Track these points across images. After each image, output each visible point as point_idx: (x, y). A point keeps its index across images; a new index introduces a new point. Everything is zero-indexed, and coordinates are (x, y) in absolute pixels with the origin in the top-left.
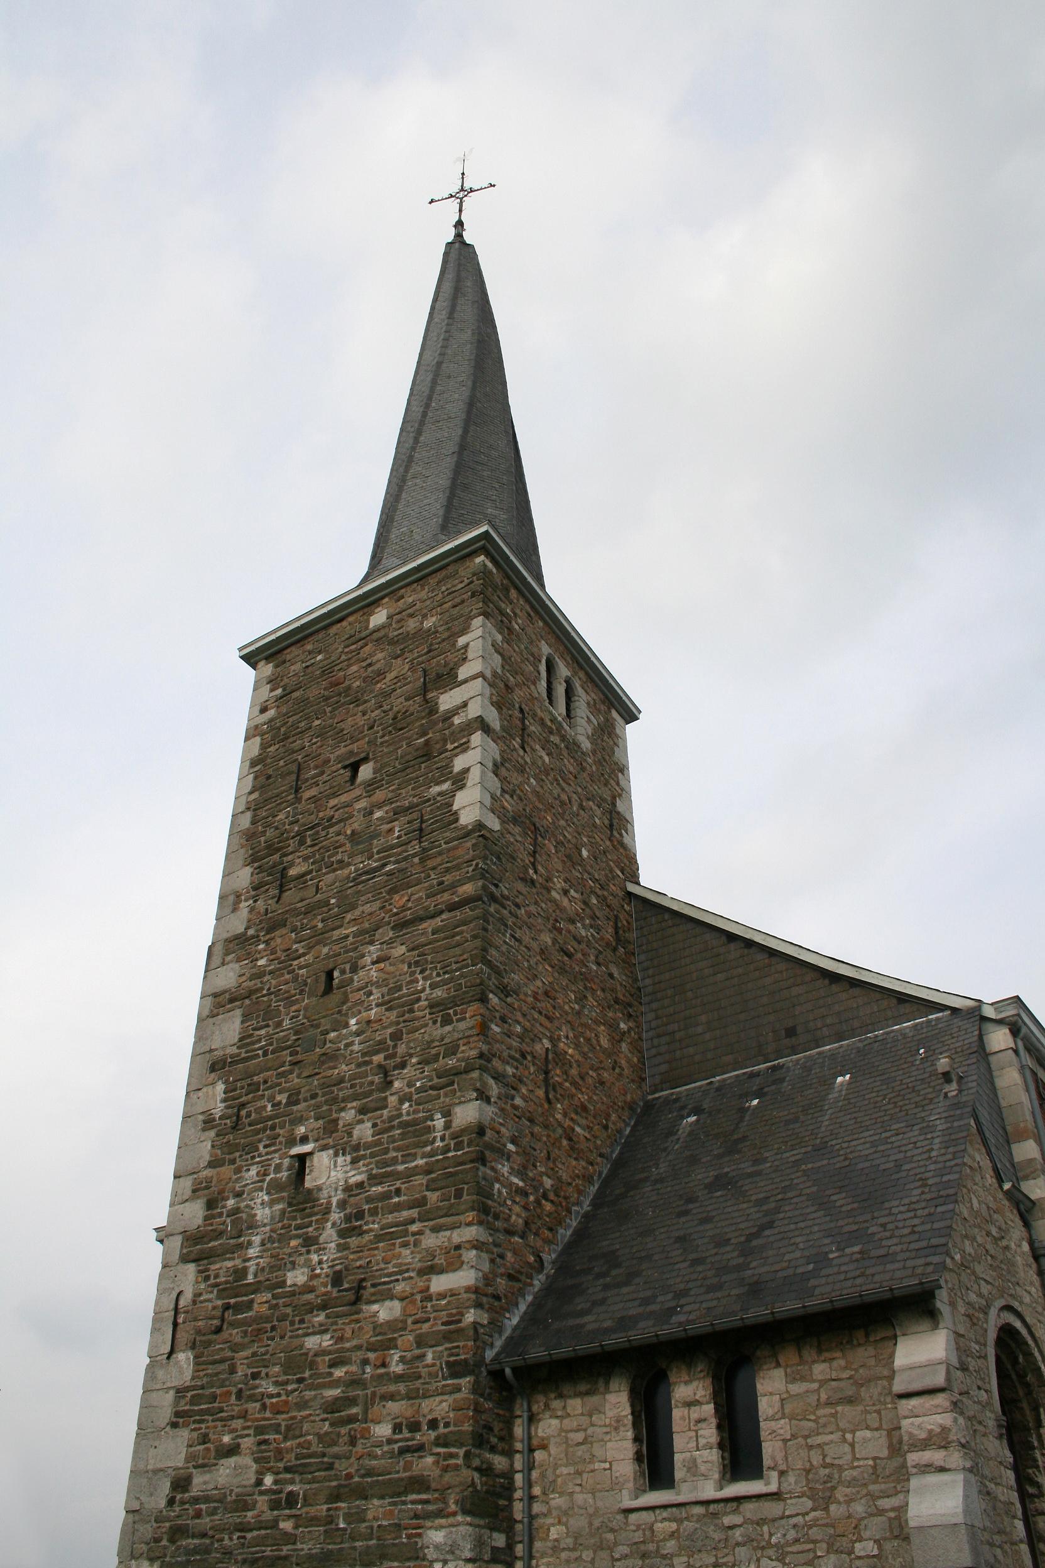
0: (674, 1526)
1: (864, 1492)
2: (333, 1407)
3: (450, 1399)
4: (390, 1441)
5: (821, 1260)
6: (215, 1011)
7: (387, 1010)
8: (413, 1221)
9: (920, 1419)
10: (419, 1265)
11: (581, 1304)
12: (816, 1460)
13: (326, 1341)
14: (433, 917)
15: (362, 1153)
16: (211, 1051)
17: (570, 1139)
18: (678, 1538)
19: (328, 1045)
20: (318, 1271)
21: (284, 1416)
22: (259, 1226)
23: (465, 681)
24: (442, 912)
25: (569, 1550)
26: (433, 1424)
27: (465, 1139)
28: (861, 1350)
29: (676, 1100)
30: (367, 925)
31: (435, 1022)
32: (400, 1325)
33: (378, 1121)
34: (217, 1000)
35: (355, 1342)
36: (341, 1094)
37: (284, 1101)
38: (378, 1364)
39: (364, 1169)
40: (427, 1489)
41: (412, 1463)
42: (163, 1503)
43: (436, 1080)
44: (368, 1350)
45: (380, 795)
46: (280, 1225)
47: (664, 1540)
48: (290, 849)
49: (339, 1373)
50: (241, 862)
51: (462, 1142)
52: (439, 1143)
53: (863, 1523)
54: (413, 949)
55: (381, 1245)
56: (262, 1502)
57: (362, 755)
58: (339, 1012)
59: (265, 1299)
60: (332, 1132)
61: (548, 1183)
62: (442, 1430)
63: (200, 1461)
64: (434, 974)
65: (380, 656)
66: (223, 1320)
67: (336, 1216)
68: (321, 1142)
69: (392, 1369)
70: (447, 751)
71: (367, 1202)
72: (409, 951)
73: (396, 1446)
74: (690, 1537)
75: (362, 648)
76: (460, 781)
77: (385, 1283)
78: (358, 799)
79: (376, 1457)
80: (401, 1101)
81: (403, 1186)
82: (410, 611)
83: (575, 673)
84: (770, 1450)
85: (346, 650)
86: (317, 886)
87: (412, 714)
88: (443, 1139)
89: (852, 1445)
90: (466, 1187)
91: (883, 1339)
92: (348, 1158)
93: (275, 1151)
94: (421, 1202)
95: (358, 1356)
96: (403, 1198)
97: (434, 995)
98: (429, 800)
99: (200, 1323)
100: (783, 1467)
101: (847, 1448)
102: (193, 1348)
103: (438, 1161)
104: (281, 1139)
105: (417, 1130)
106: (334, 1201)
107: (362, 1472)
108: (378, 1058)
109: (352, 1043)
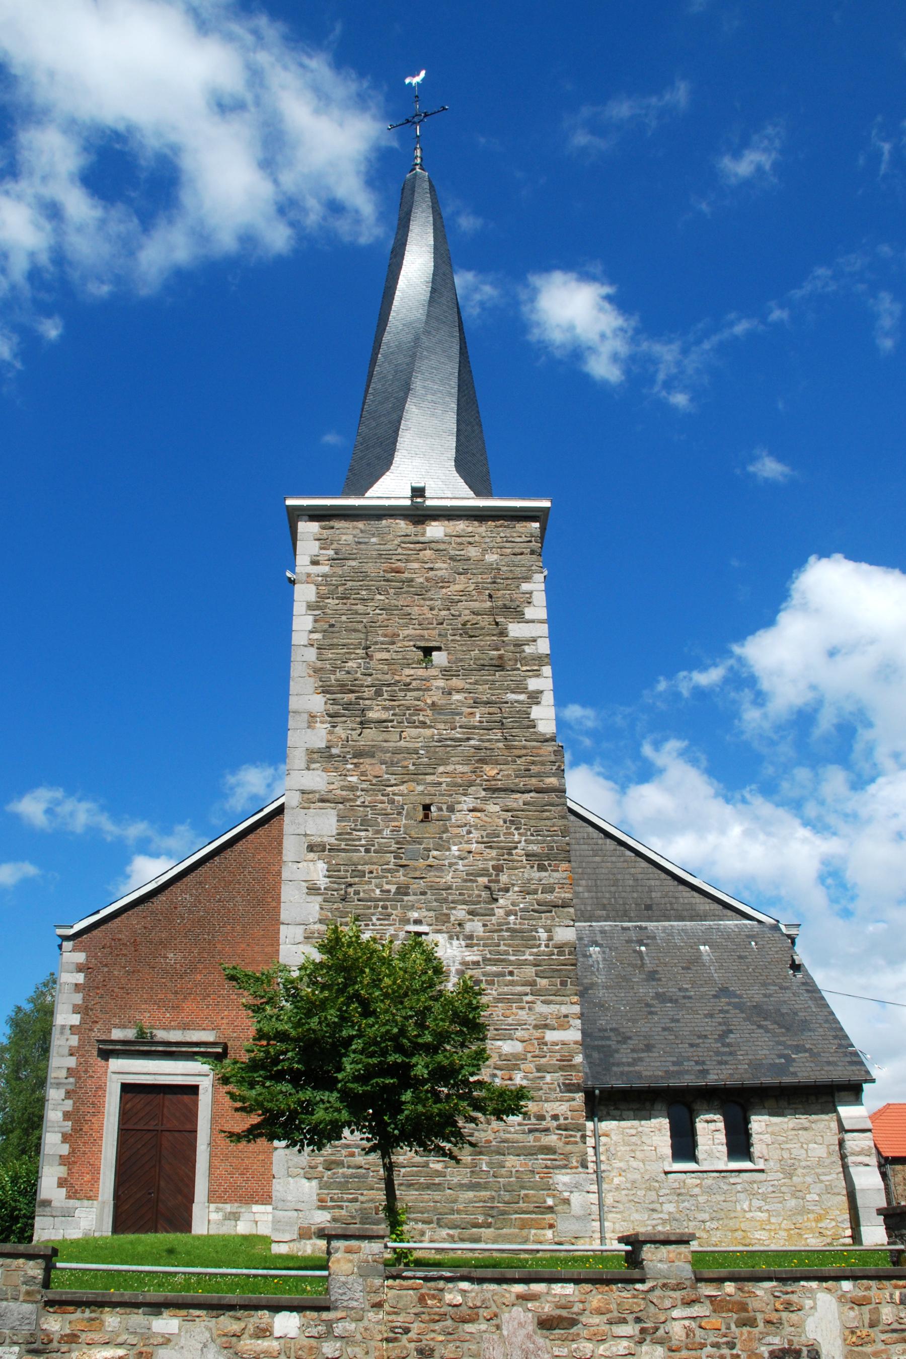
0: (698, 1181)
3: (567, 1104)
5: (789, 1060)
6: (306, 805)
7: (485, 847)
8: (527, 994)
10: (534, 1022)
12: (786, 1155)
14: (523, 793)
15: (475, 941)
16: (306, 835)
19: (431, 859)
23: (533, 621)
24: (531, 791)
25: (628, 1189)
26: (555, 1117)
30: (459, 780)
31: (532, 867)
32: (523, 1057)
33: (488, 923)
34: (306, 796)
36: (450, 898)
37: (393, 890)
38: (506, 1077)
40: (555, 1153)
41: (540, 1138)
43: (536, 907)
44: (495, 1068)
45: (456, 682)
48: (366, 695)
50: (312, 690)
52: (543, 948)
54: (507, 811)
55: (500, 1005)
64: (529, 833)
71: (484, 976)
74: (709, 1187)
75: (420, 550)
76: (535, 697)
78: (435, 678)
79: (510, 1133)
80: (508, 914)
82: (470, 539)
84: (757, 1149)
85: (403, 545)
86: (401, 736)
87: (483, 628)
88: (547, 946)
89: (806, 1151)
90: (569, 980)
91: (826, 1102)
92: (463, 943)
93: (390, 925)
94: (533, 984)
98: (506, 703)
100: (767, 1157)
101: (804, 1152)
104: (393, 917)
105: (525, 938)
107: (499, 1140)
108: (483, 880)
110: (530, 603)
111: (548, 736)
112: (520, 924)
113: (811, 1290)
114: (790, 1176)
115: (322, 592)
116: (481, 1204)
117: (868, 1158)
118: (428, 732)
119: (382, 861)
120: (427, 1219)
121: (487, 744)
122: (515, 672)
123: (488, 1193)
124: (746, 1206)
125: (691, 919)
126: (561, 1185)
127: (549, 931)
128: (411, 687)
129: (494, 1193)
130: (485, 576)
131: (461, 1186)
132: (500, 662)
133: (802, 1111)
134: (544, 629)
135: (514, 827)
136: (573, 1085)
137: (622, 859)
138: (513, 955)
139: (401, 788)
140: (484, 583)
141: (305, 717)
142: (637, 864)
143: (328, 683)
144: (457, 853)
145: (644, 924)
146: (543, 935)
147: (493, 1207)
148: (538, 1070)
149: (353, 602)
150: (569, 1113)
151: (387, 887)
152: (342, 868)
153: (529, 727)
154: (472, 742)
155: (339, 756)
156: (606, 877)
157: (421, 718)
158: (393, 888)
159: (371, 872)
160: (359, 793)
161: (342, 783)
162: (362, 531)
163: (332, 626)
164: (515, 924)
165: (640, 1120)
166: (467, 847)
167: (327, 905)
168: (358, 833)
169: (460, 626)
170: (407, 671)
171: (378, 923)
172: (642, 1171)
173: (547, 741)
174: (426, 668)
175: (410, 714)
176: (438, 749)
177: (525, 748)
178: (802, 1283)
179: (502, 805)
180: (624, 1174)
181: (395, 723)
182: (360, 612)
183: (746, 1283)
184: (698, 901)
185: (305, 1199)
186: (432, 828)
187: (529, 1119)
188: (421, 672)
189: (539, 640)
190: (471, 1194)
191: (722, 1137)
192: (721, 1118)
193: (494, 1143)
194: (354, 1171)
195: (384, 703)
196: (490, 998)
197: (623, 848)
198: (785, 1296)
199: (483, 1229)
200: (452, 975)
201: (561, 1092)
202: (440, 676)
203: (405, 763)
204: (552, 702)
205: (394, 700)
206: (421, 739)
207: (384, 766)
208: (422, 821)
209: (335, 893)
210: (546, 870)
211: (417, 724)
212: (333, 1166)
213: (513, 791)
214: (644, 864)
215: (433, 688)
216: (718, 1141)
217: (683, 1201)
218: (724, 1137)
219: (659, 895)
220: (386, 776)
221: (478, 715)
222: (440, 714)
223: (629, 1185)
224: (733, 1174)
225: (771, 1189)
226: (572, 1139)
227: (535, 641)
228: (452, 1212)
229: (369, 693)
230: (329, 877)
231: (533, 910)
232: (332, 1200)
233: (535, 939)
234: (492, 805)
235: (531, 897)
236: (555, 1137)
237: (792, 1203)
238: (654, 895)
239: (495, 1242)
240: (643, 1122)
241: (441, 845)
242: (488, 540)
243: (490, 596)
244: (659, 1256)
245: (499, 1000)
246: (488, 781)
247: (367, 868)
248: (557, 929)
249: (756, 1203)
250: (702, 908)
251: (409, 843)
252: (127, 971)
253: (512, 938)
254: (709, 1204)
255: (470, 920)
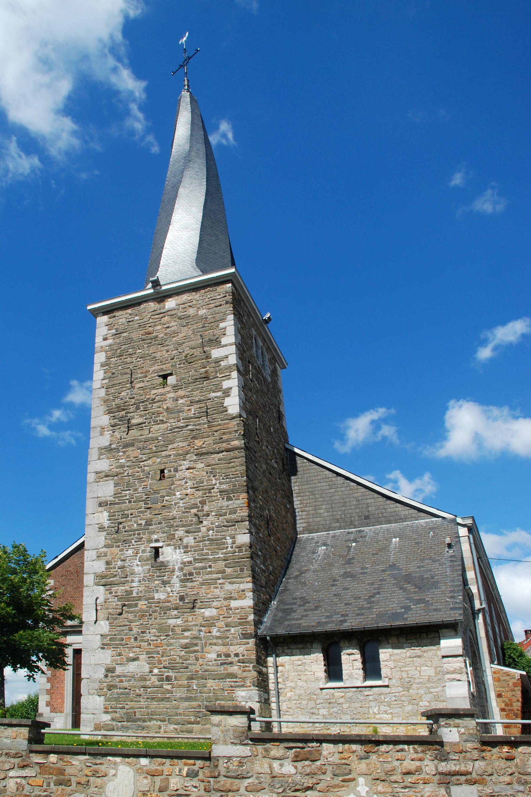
0: (343, 694)
1: (424, 686)
2: (185, 647)
4: (215, 660)
5: (407, 608)
6: (98, 480)
7: (196, 490)
8: (220, 579)
9: (451, 664)
10: (224, 596)
11: (295, 615)
12: (404, 675)
13: (179, 621)
14: (218, 453)
15: (189, 549)
16: (98, 497)
17: (276, 551)
18: (345, 698)
19: (165, 502)
20: (171, 595)
21: (161, 648)
22: (137, 574)
23: (226, 346)
24: (223, 452)
26: (237, 655)
27: (244, 549)
28: (424, 640)
29: (312, 539)
30: (181, 452)
31: (223, 499)
32: (217, 618)
33: (197, 537)
34: (98, 475)
35: (194, 623)
37: (144, 524)
38: (207, 631)
39: (192, 556)
40: (236, 677)
41: (227, 668)
42: (102, 676)
44: (201, 626)
45: (181, 393)
46: (148, 574)
47: (338, 698)
48: (131, 410)
49: (186, 634)
50: (102, 413)
51: (242, 549)
52: (229, 549)
53: (423, 696)
54: (208, 466)
55: (203, 587)
56: (154, 679)
57: (169, 372)
58: (170, 488)
59: (144, 603)
60: (172, 539)
61: (271, 568)
62: (241, 657)
63: (119, 662)
64: (221, 478)
65: (173, 324)
66: (122, 610)
67: (177, 573)
68: (166, 543)
69: (214, 634)
70: (218, 377)
71: (194, 569)
72: (206, 466)
73: (219, 662)
74: (350, 698)
75: (162, 318)
76: (227, 393)
77: (207, 602)
78: (169, 392)
79: (209, 665)
80: (208, 530)
81: (213, 565)
82: (190, 304)
83: (264, 344)
85: (152, 317)
86: (150, 431)
87: (197, 356)
88: (232, 547)
89: (420, 672)
90: (245, 568)
92: (182, 551)
93: (142, 544)
94: (224, 572)
95: (197, 628)
96: (213, 569)
97: (222, 487)
98: (210, 399)
99: (110, 610)
100: (391, 677)
101: (417, 672)
102: (108, 619)
103: (230, 556)
104: (144, 539)
105: (218, 543)
106: (176, 567)
107: (203, 670)
108: (194, 511)
109: (179, 503)
110: (225, 334)
111: (234, 415)
112: (216, 535)
113: (115, 763)
114: (408, 690)
115: (108, 355)
116: (193, 710)
117: (460, 675)
118: (164, 426)
119: (138, 507)
120: (162, 719)
121: (198, 427)
122: (216, 379)
123: (197, 703)
124: (376, 710)
125: (396, 521)
126: (240, 698)
127: (233, 537)
128: (155, 400)
129: (200, 703)
130: (197, 325)
131: (181, 698)
132: (206, 374)
133: (417, 644)
134: (233, 349)
135: (212, 475)
136: (248, 634)
137: (348, 488)
138: (211, 555)
139: (148, 462)
140: (197, 328)
141: (99, 429)
142: (358, 491)
143: (111, 407)
144: (179, 496)
145: (363, 529)
146: (229, 541)
147: (200, 712)
148: (227, 626)
149: (125, 357)
150: (245, 652)
151: (140, 522)
152: (116, 514)
153: (223, 412)
154: (189, 427)
155: (116, 449)
156: (338, 501)
157: (161, 418)
158: (143, 522)
159: (132, 514)
160: (125, 469)
161: (117, 464)
162: (130, 315)
163: (113, 374)
164: (212, 536)
165: (304, 655)
166: (185, 492)
167: (109, 537)
168: (125, 492)
169: (184, 358)
170: (153, 392)
171: (135, 544)
172: (305, 688)
173: (233, 418)
174: (164, 387)
175: (155, 417)
176: (169, 435)
177: (219, 425)
178: (109, 758)
179: (205, 463)
180: (293, 690)
181: (147, 424)
182: (128, 362)
183: (65, 756)
184: (400, 509)
185: (97, 707)
186: (165, 483)
187: (221, 657)
188: (161, 391)
189: (230, 357)
190: (187, 703)
191: (359, 664)
192: (358, 652)
193: (200, 672)
194: (123, 691)
195: (140, 413)
196: (198, 583)
197: (348, 481)
198: (95, 766)
199: (195, 725)
200: (176, 571)
201: (240, 639)
202: (172, 391)
203: (150, 447)
204: (237, 393)
205: (146, 410)
206: (161, 431)
207: (139, 450)
208: (160, 479)
209: (113, 529)
210: (232, 500)
211: (158, 422)
212: (111, 688)
213: (212, 453)
214: (363, 490)
215: (168, 398)
216: (356, 667)
217: (333, 707)
218: (361, 664)
219: (374, 508)
220: (140, 456)
221: (193, 410)
222: (171, 413)
223: (297, 697)
224: (367, 689)
225: (394, 698)
226: (247, 668)
227: (227, 357)
228: (177, 714)
229: (132, 409)
230: (109, 520)
231: (223, 526)
232: (111, 708)
233: (225, 544)
234: (200, 464)
235: (223, 517)
236: (236, 667)
237: (409, 708)
238: (370, 509)
239: (201, 733)
240: (306, 656)
241: (170, 493)
242: (200, 302)
243: (201, 336)
244: (6, 734)
245: (202, 584)
246: (197, 449)
247: (129, 512)
248: (238, 536)
249: (383, 708)
250: (403, 513)
251: (152, 494)
252: (74, 588)
253: (211, 545)
254: (350, 709)
255: (186, 536)
